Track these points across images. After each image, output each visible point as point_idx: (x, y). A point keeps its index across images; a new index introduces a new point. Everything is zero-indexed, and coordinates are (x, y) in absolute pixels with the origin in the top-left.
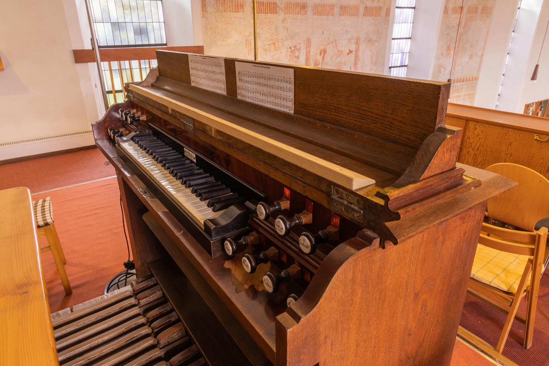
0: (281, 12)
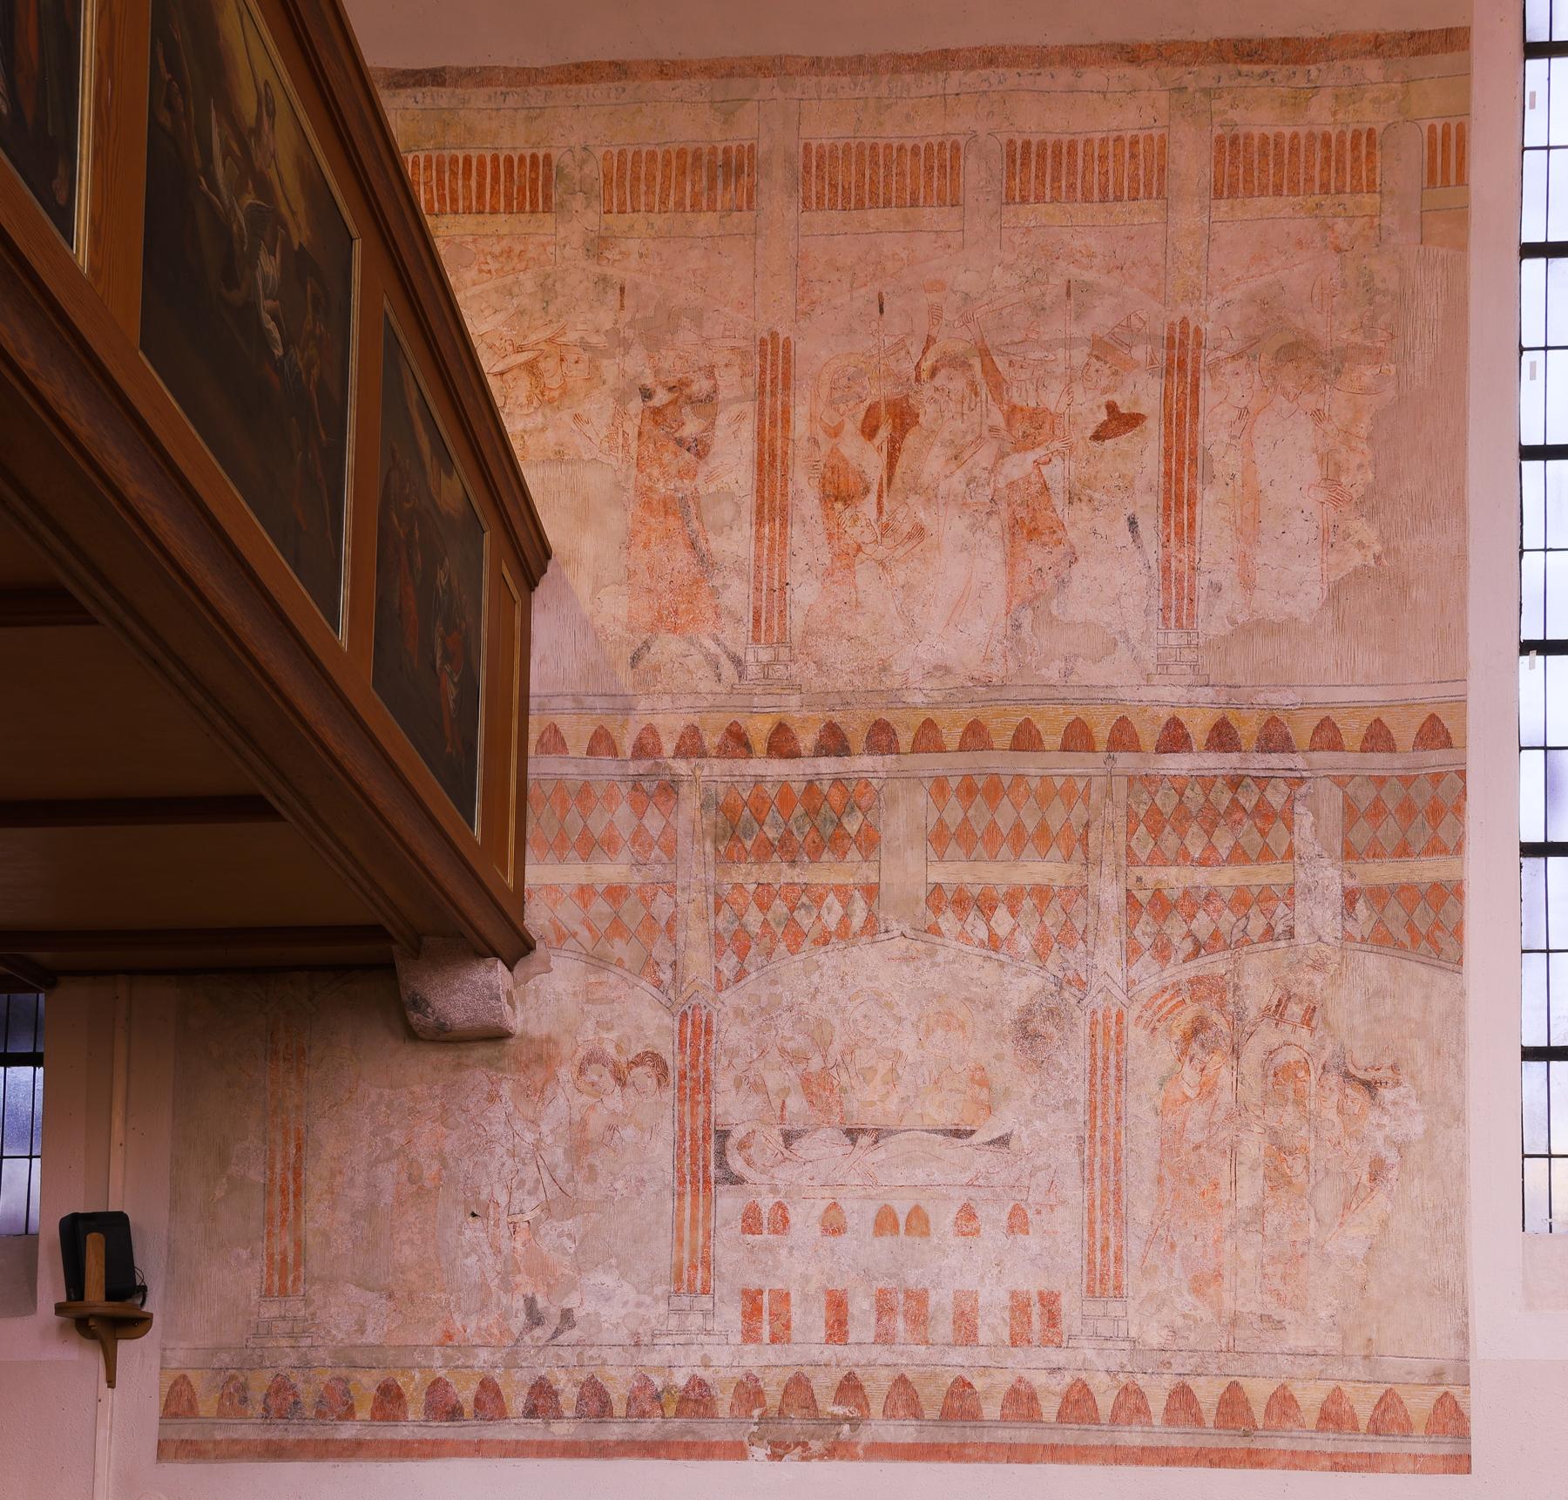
0: (577, 203)
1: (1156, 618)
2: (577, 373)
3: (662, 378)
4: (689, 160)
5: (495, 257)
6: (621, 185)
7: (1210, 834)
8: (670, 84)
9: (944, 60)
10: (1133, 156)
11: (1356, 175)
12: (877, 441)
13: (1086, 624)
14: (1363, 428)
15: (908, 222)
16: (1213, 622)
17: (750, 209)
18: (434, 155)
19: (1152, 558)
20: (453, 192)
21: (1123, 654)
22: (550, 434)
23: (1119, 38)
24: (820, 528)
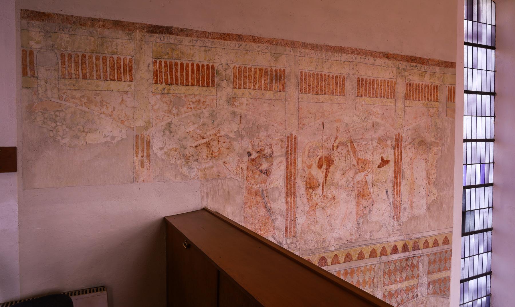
0: (224, 84)
1: (392, 218)
2: (224, 146)
3: (255, 148)
4: (263, 72)
5: (193, 103)
6: (240, 79)
7: (401, 274)
8: (257, 45)
9: (340, 50)
10: (388, 86)
11: (434, 97)
12: (322, 170)
13: (376, 222)
14: (434, 164)
15: (331, 100)
16: (404, 219)
17: (283, 91)
18: (168, 61)
19: (391, 201)
20: (176, 77)
21: (384, 229)
22: (215, 169)
23: (384, 51)
24: (305, 198)
